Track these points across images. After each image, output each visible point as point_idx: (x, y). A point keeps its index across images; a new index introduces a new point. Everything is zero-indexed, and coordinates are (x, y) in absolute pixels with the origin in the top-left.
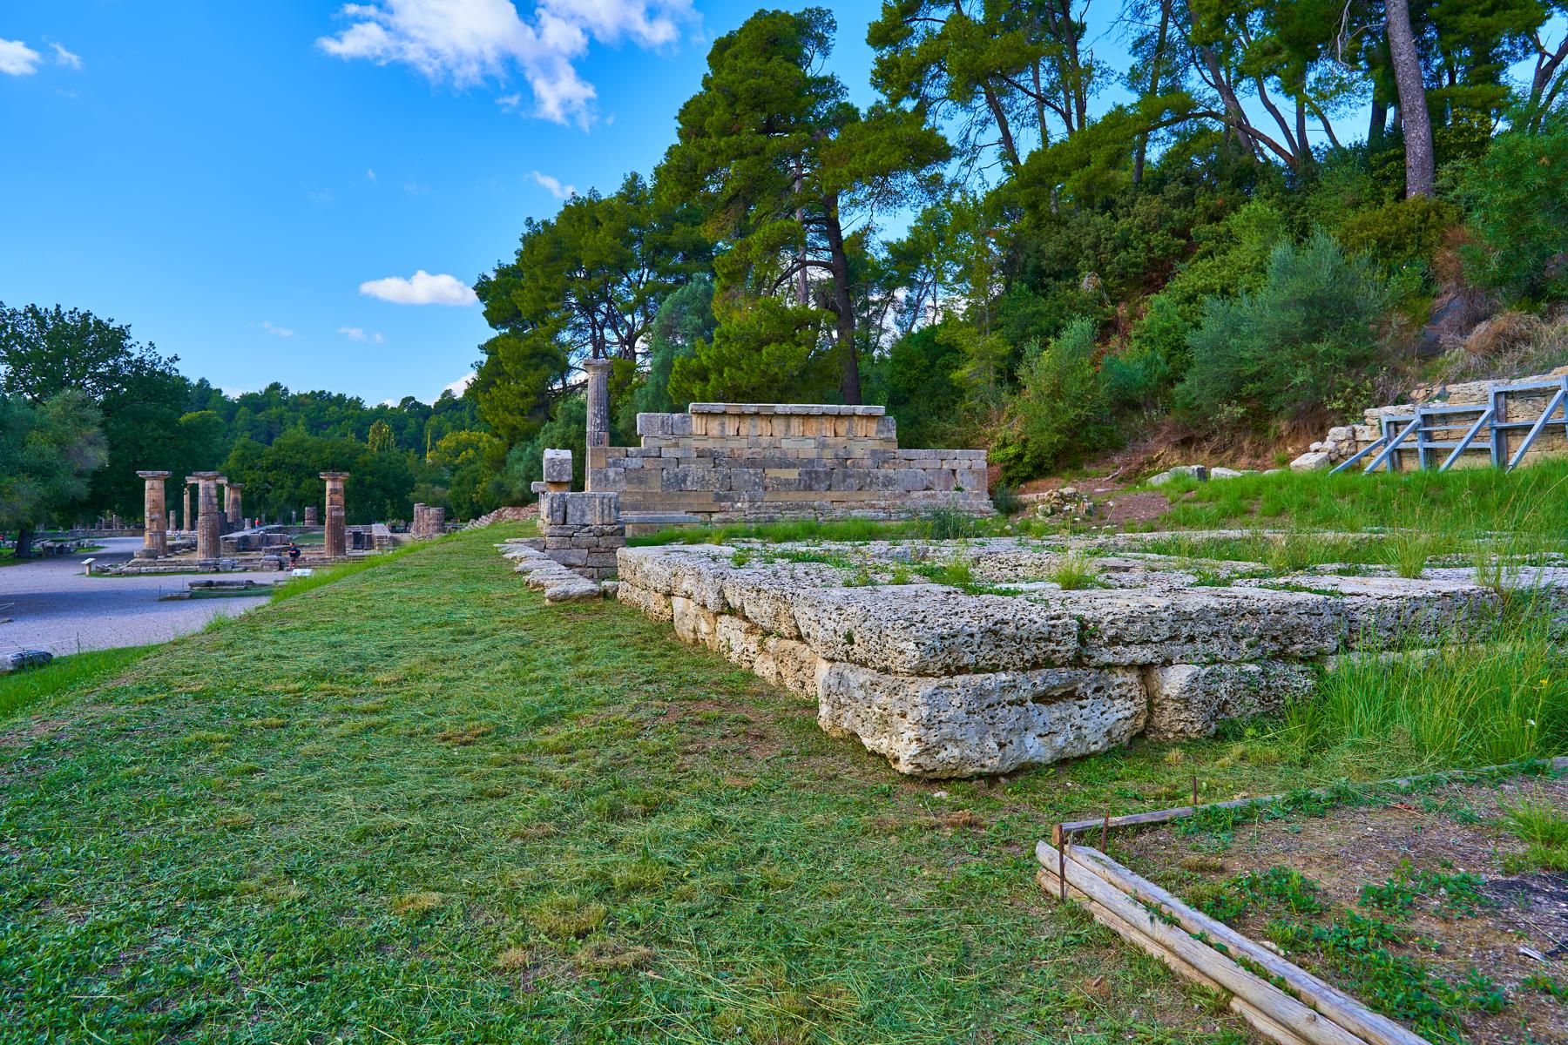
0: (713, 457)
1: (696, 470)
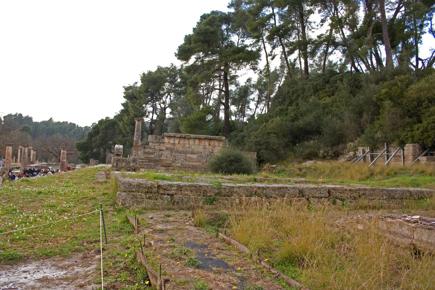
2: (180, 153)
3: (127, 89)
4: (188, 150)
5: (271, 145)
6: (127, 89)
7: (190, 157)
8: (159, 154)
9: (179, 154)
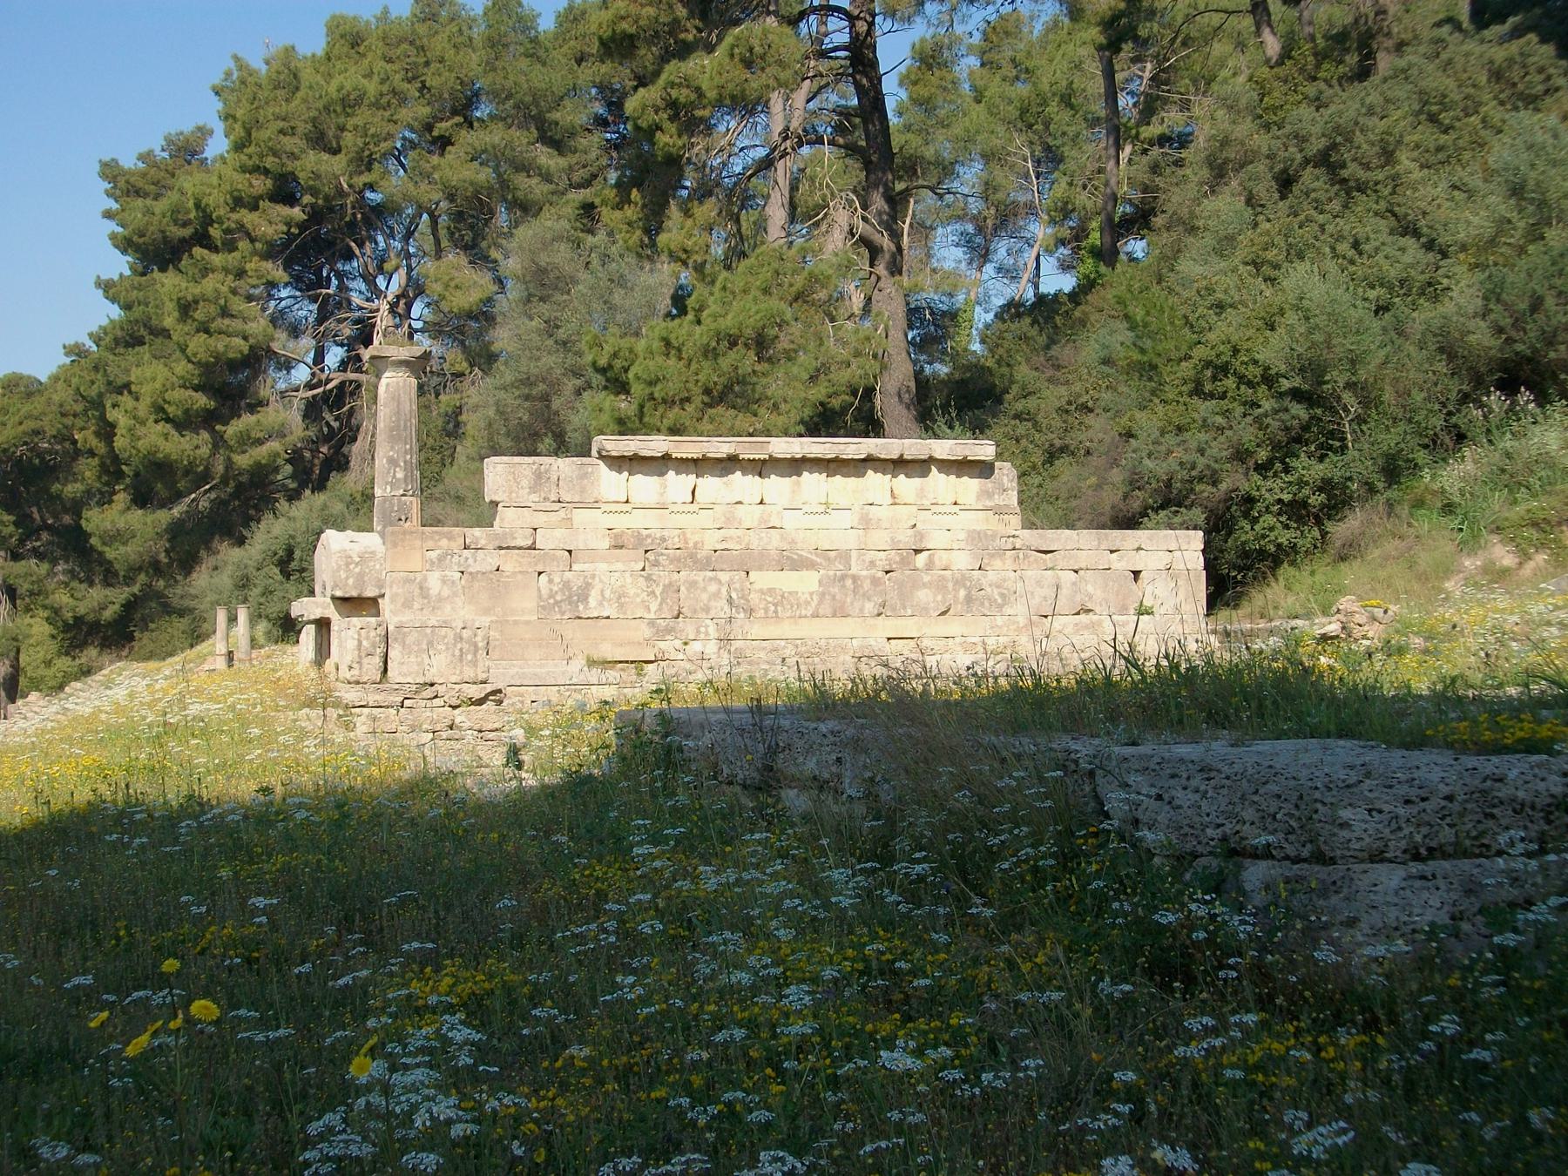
0: (645, 548)
1: (612, 577)
2: (707, 565)
3: (126, 186)
4: (755, 541)
5: (147, 356)
6: (126, 186)
7: (771, 591)
8: (566, 585)
9: (699, 576)
